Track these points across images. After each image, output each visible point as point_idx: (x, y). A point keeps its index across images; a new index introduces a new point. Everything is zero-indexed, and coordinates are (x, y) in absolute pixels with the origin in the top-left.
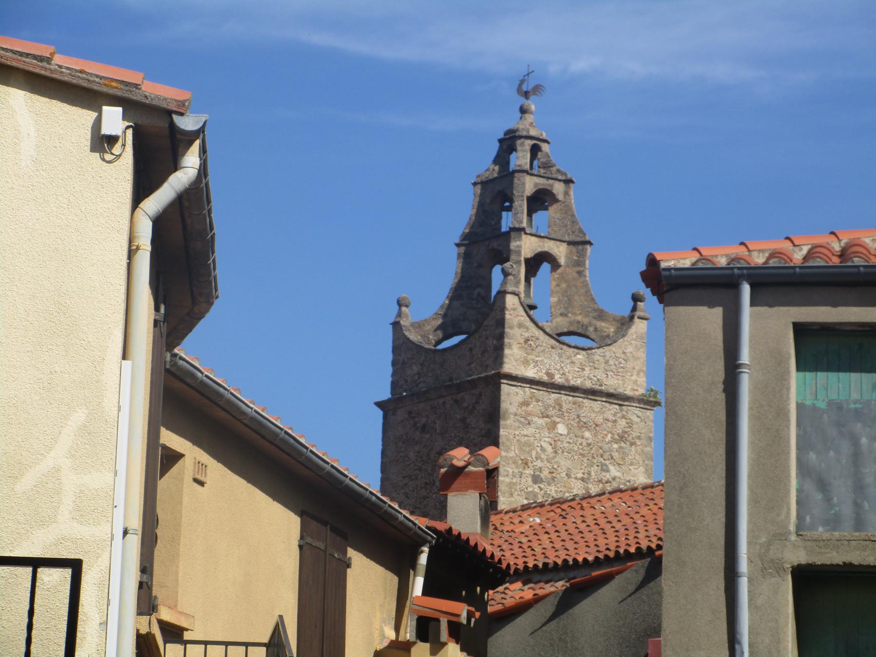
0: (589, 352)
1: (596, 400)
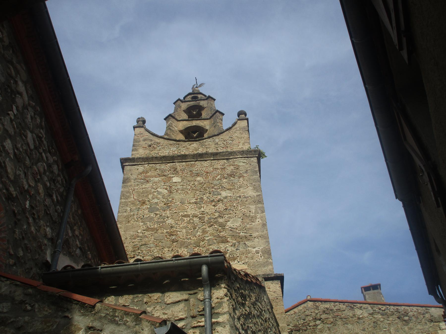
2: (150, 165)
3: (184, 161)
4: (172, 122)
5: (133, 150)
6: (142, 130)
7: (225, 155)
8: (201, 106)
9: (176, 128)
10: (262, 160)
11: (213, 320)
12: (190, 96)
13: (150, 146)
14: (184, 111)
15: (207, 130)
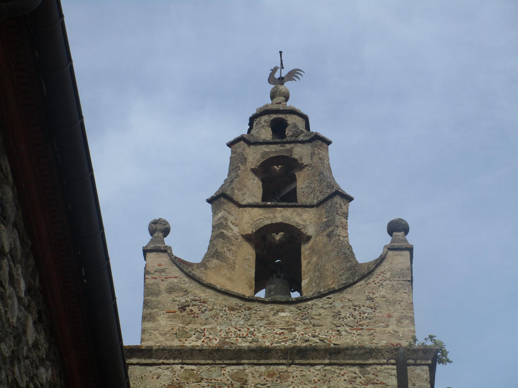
0: (303, 305)
1: (313, 365)
2: (186, 367)
3: (262, 361)
4: (227, 215)
5: (144, 318)
6: (163, 259)
7: (356, 355)
8: (295, 160)
9: (236, 230)
10: (439, 367)
11: (146, 277)
12: (266, 118)
13: (183, 308)
14: (253, 170)
15: (309, 238)
